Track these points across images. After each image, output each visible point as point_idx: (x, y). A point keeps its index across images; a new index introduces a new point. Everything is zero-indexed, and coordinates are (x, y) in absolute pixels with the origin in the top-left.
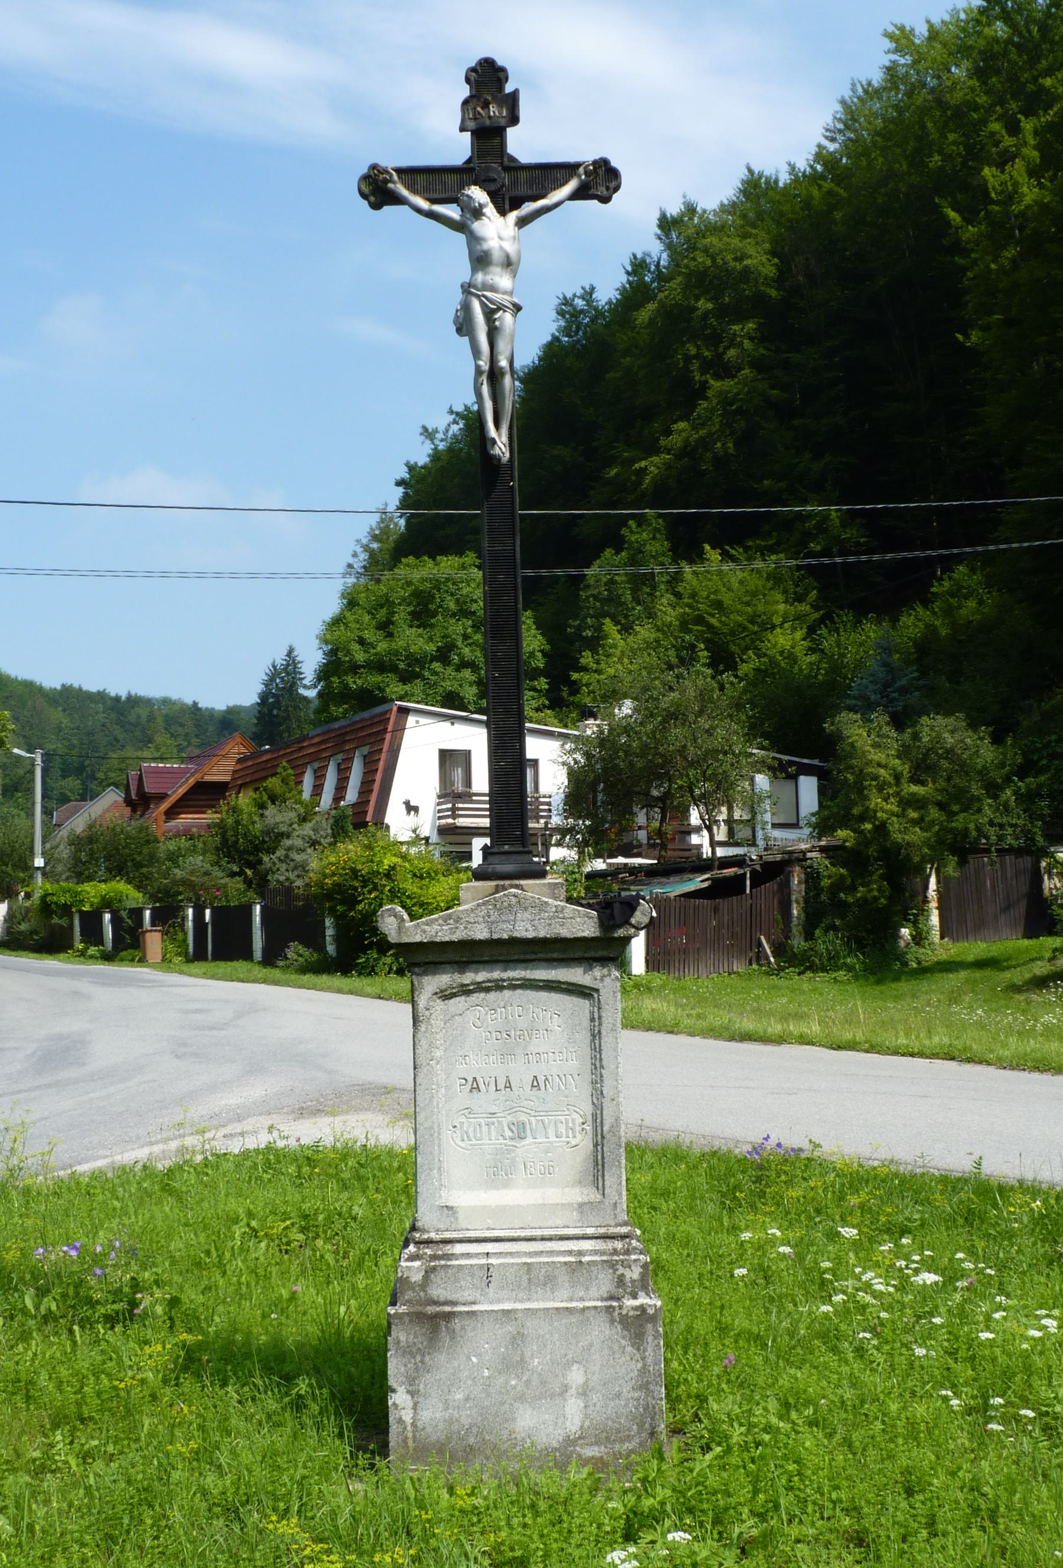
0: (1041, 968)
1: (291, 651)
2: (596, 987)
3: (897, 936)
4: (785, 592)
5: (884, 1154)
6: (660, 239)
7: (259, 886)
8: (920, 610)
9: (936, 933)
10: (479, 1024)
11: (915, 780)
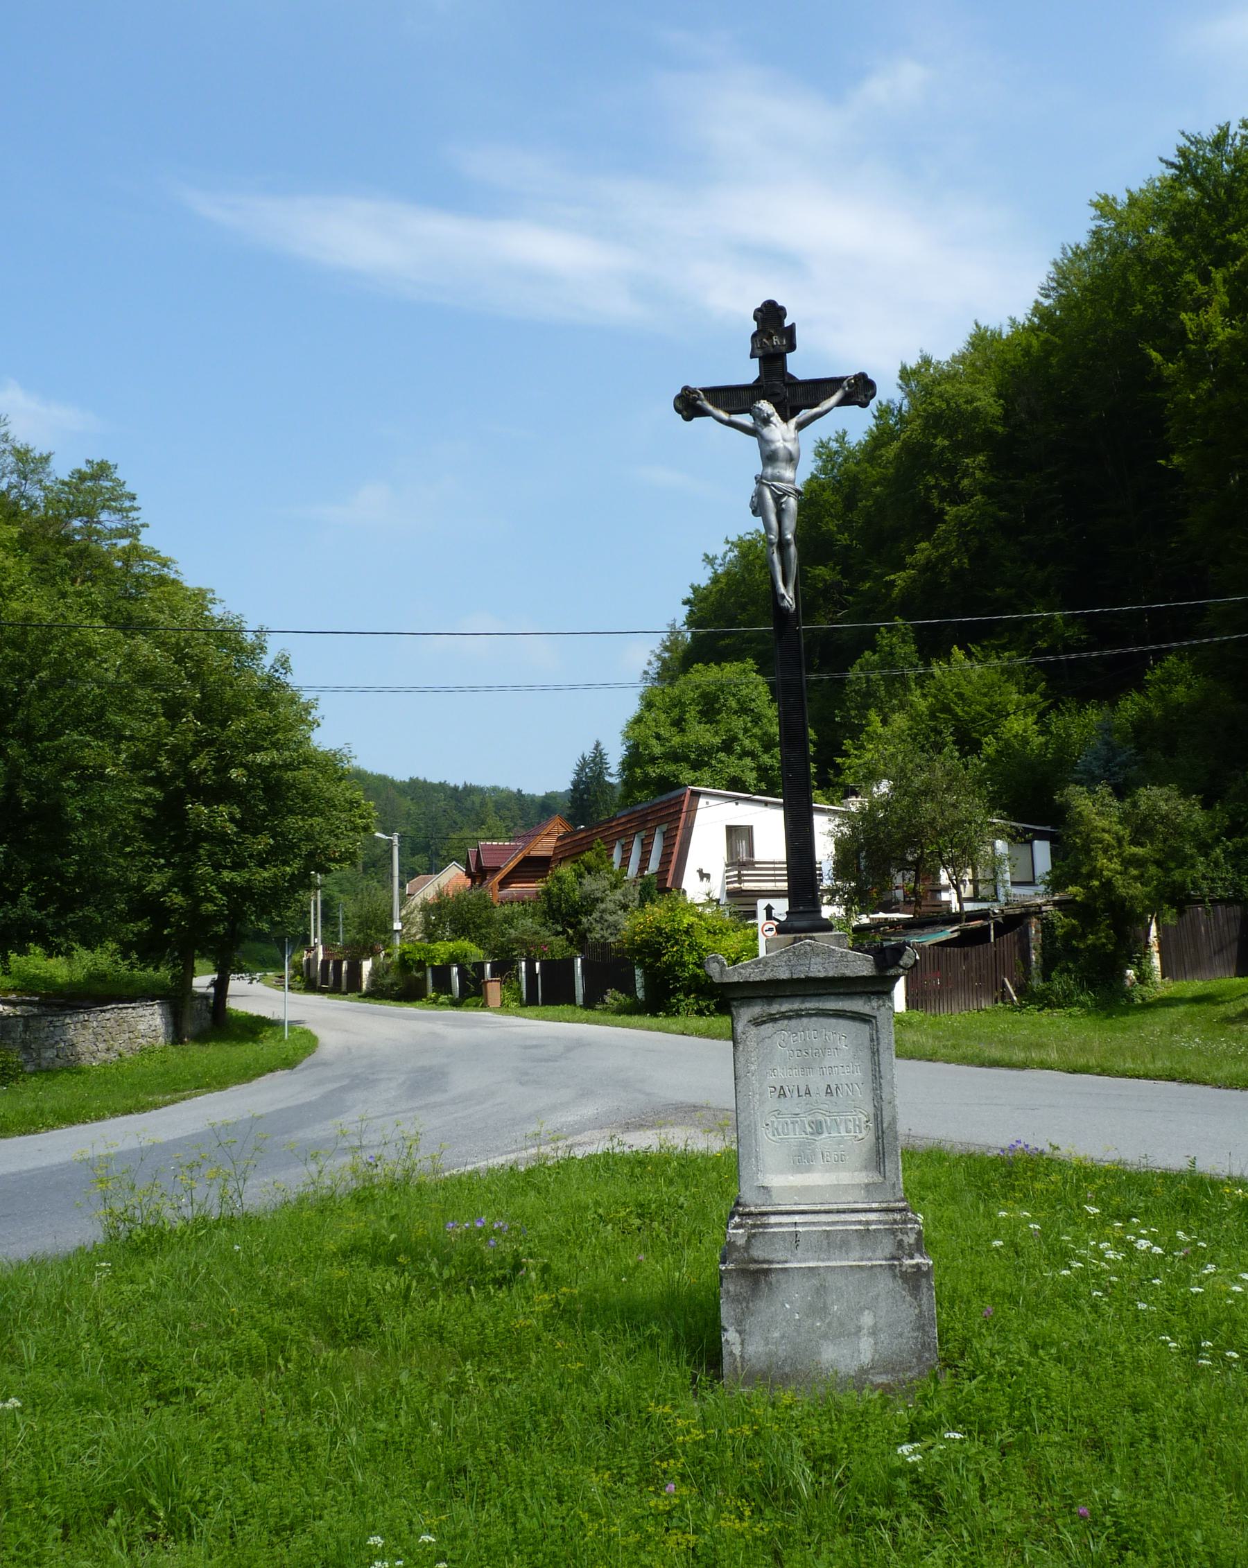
1: (598, 745)
3: (1123, 977)
4: (1017, 684)
5: (1114, 1156)
7: (579, 942)
8: (1135, 696)
11: (1135, 842)
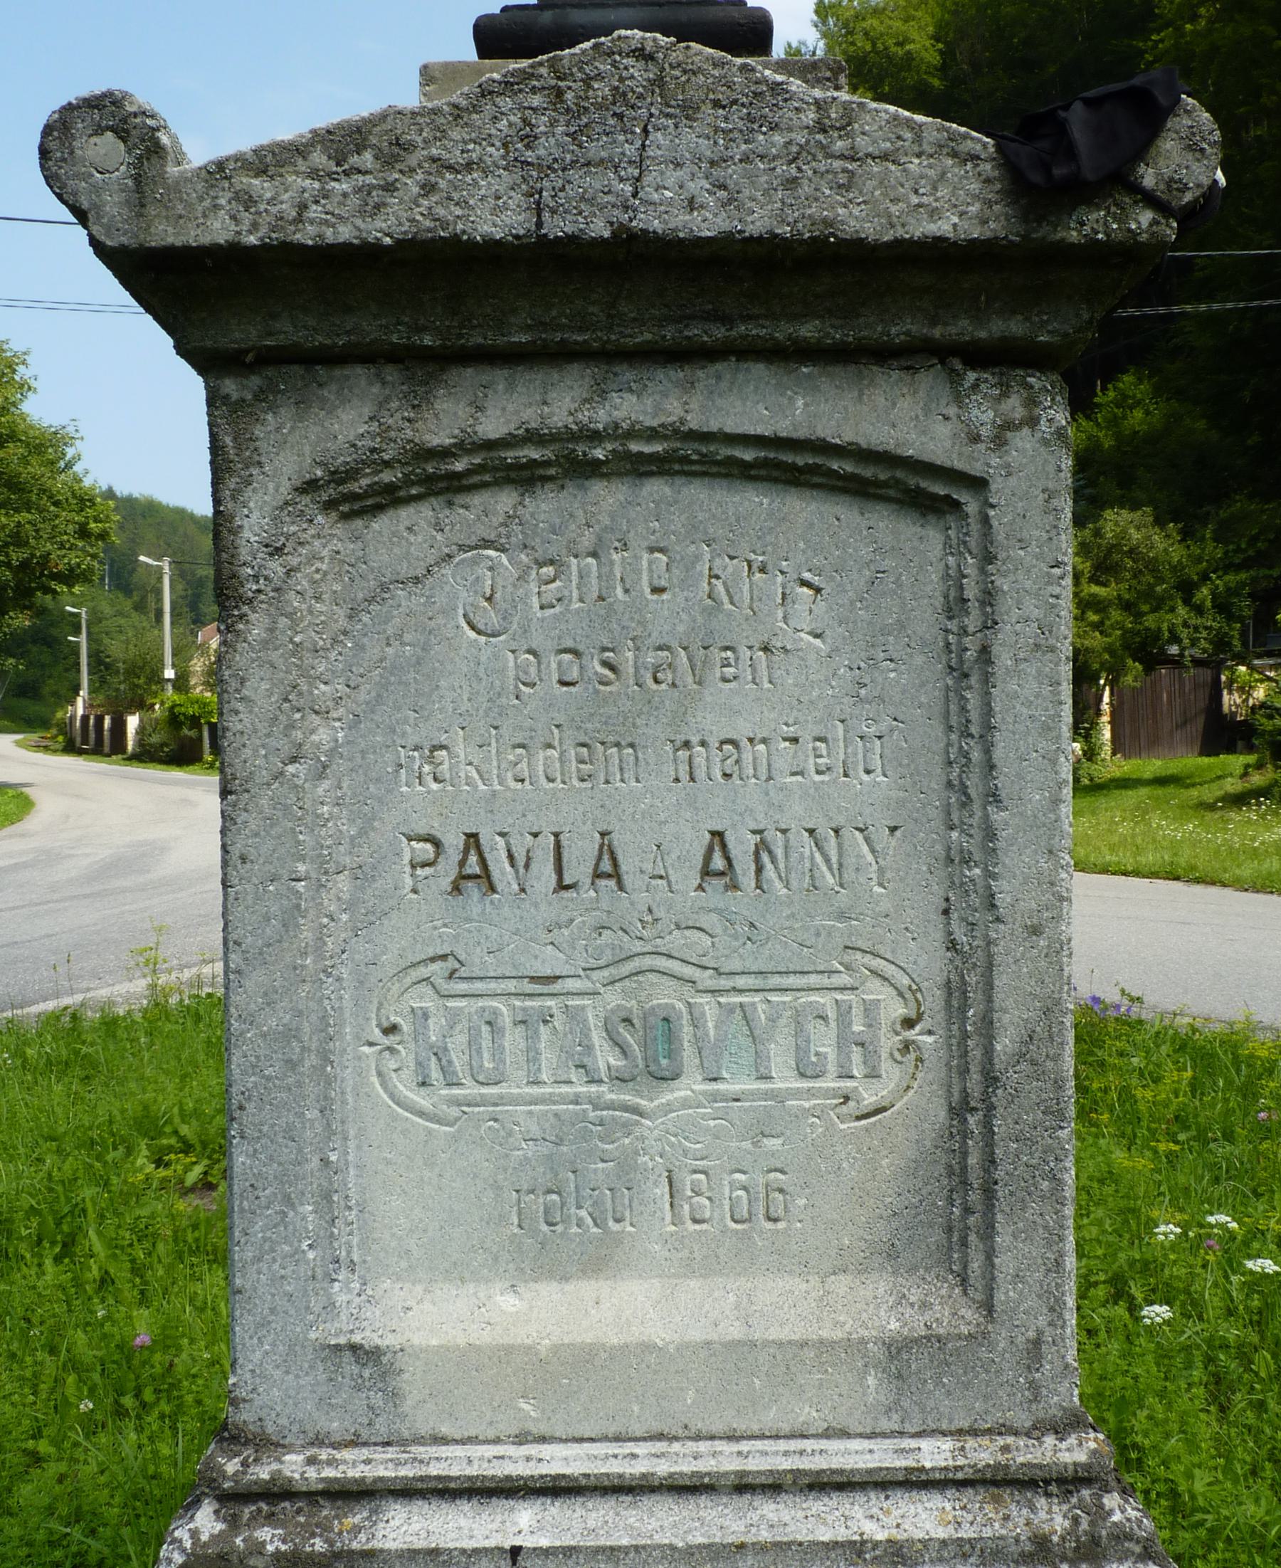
0: (1232, 785)
2: (976, 469)
6: (816, 26)
9: (1107, 749)
10: (492, 619)
11: (1094, 580)
